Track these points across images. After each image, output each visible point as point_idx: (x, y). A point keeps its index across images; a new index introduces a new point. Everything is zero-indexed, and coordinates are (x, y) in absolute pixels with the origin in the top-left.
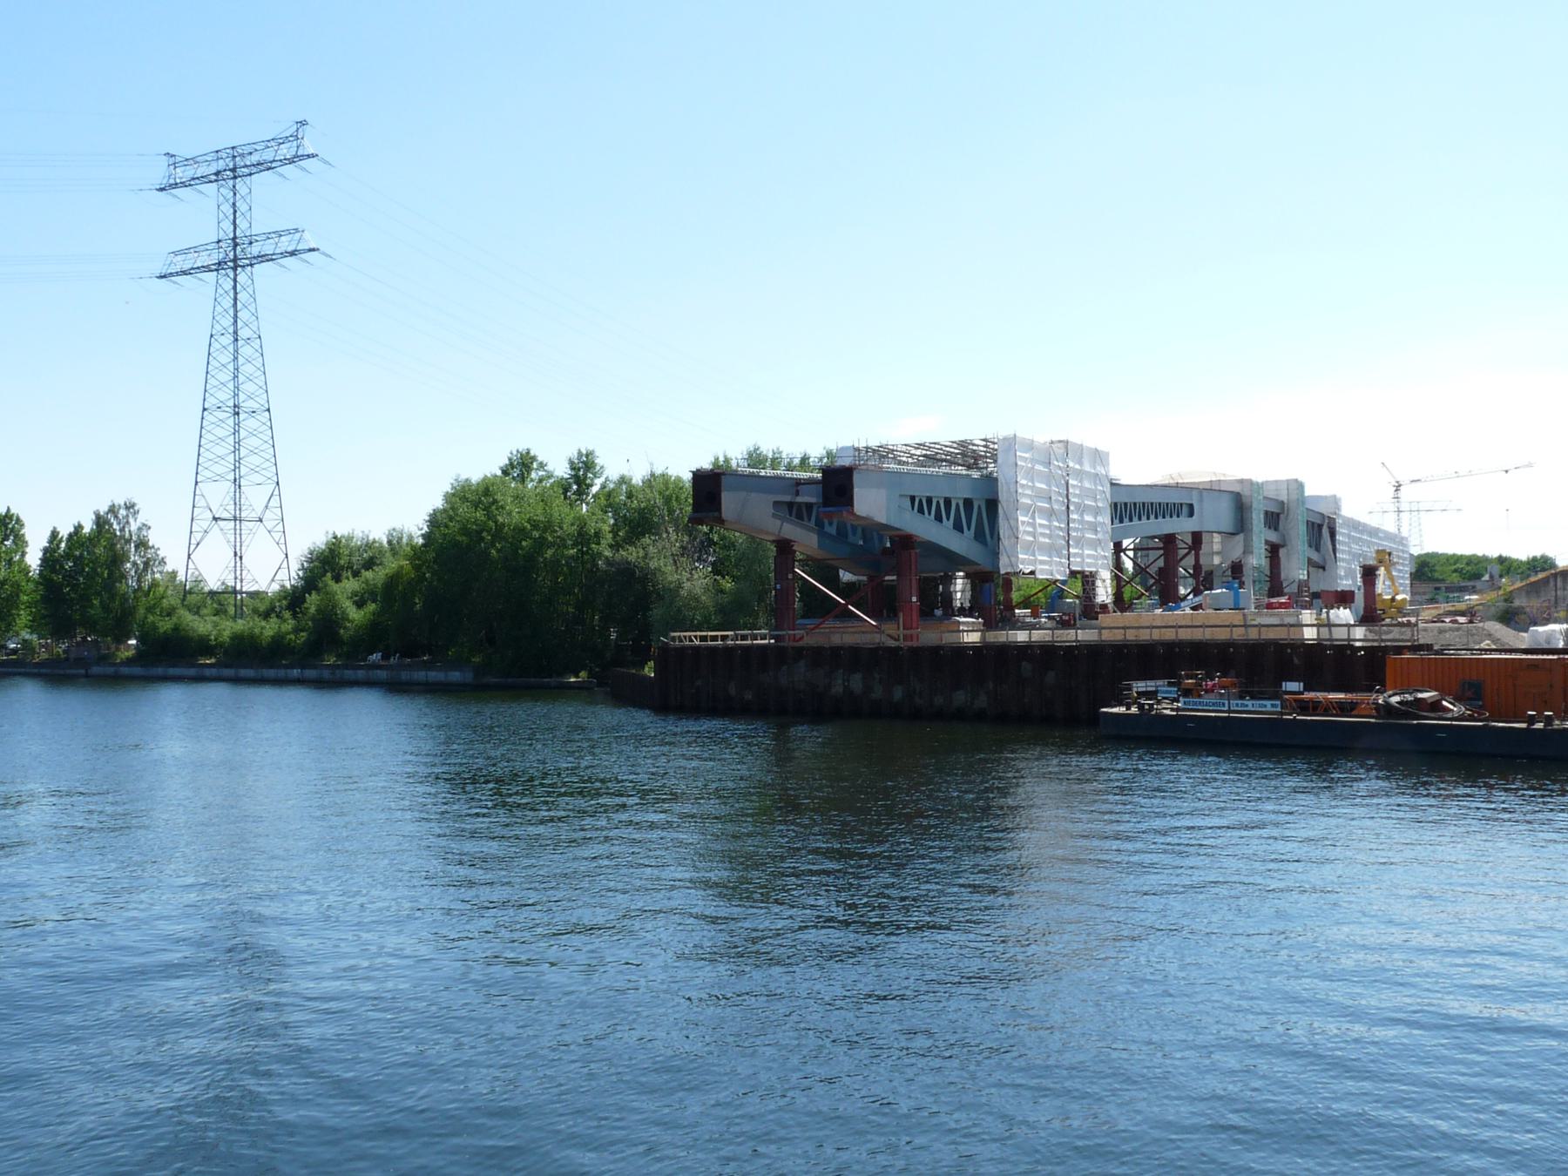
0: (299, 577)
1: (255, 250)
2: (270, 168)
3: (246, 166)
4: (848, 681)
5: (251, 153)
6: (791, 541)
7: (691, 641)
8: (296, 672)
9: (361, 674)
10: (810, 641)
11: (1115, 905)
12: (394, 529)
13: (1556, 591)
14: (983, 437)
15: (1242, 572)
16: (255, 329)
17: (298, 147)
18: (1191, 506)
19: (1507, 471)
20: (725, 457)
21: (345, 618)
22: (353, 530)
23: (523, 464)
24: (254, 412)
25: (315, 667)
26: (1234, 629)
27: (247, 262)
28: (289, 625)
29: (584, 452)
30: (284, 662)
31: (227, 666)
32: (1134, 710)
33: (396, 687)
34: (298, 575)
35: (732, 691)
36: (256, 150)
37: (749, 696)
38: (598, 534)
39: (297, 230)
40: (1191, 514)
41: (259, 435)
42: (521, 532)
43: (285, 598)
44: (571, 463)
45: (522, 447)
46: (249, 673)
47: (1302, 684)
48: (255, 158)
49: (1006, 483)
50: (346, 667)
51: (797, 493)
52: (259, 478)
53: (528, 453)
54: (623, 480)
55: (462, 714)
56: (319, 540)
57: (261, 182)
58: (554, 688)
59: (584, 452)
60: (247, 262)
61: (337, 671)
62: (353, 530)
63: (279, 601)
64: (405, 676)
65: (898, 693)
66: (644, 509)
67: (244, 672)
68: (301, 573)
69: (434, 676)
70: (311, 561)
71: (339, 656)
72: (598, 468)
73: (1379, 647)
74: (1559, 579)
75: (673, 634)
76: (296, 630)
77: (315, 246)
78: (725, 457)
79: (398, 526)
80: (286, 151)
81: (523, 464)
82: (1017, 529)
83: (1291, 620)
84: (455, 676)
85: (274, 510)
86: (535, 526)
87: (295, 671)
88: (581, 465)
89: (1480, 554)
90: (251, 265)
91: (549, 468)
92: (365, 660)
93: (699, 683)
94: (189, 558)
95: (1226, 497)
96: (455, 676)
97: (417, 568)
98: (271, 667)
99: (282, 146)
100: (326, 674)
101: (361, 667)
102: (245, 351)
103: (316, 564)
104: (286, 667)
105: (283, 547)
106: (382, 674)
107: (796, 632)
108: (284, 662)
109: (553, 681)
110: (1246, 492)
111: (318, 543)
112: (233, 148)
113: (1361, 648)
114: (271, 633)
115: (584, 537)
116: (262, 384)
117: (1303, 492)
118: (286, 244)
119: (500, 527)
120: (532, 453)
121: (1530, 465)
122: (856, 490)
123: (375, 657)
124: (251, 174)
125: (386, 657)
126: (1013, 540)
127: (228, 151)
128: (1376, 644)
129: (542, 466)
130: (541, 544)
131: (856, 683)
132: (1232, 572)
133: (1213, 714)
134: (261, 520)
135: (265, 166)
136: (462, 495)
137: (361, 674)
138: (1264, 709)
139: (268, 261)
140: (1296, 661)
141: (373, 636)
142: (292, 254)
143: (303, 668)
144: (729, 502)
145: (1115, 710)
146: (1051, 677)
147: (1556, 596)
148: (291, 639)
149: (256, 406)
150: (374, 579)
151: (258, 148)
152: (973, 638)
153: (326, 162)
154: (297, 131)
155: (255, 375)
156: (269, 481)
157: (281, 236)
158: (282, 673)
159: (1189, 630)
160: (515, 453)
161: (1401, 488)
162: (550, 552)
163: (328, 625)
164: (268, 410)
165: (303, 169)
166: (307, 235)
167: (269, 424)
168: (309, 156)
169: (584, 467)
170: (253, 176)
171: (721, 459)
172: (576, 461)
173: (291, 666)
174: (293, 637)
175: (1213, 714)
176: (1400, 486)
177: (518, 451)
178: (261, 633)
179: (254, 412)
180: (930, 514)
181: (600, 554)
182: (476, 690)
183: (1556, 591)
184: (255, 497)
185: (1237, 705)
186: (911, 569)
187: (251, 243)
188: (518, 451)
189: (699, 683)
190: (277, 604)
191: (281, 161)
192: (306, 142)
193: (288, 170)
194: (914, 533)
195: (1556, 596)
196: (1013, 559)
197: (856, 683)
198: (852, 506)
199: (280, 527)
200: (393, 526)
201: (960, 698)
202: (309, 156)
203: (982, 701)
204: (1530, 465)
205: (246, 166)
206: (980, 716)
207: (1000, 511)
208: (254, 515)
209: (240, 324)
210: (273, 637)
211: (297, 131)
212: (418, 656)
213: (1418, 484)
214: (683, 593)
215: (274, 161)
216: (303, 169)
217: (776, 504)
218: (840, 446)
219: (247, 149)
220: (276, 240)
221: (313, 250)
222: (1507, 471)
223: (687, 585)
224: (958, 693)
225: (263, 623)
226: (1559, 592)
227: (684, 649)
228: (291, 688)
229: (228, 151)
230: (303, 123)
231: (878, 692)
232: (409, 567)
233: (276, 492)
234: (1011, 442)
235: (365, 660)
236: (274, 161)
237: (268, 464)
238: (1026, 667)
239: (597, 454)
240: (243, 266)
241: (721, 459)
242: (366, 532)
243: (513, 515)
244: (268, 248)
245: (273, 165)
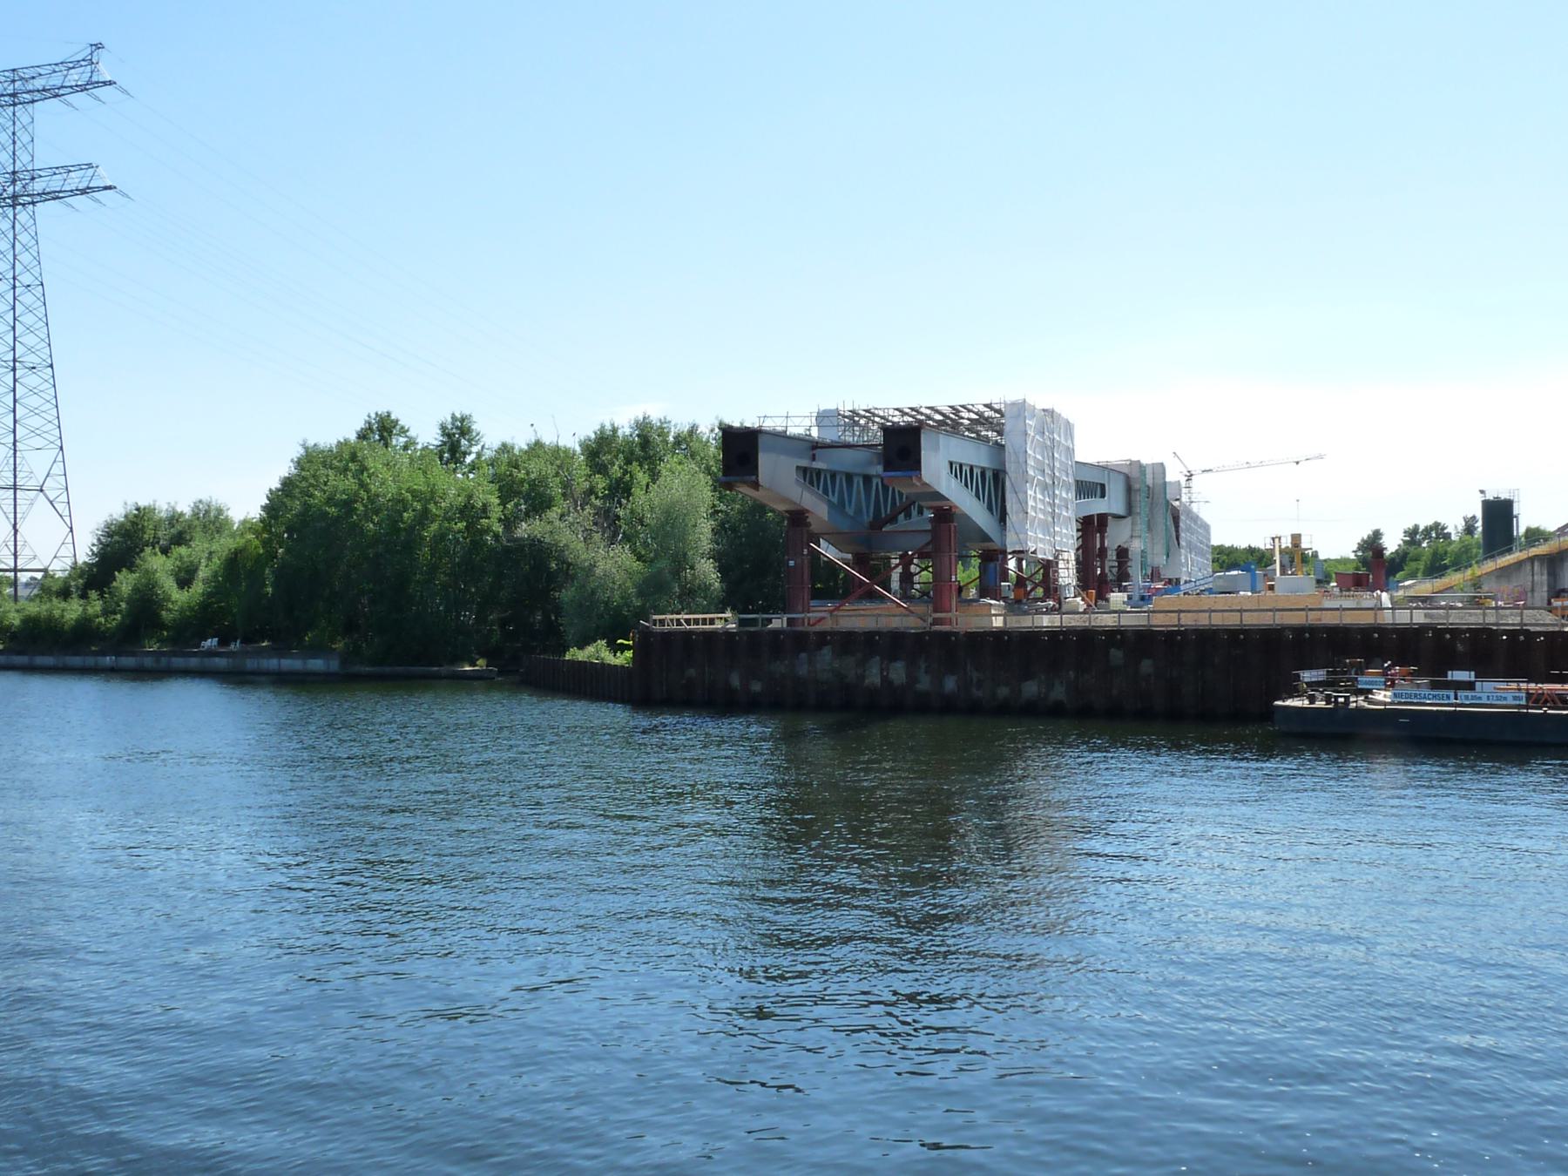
0: (93, 554)
1: (38, 186)
2: (57, 96)
3: (29, 92)
4: (888, 670)
5: (33, 78)
6: (808, 511)
7: (681, 625)
8: (108, 660)
9: (194, 662)
10: (827, 625)
11: (1354, 934)
12: (200, 501)
13: (1533, 575)
14: (988, 402)
15: (1127, 557)
16: (37, 275)
17: (92, 72)
18: (1103, 486)
19: (1297, 463)
20: (613, 425)
21: (168, 599)
22: (155, 501)
23: (383, 428)
24: (34, 368)
25: (133, 654)
26: (1309, 613)
27: (29, 199)
28: (96, 606)
29: (459, 416)
30: (93, 648)
31: (20, 653)
32: (1320, 704)
33: (236, 678)
34: (92, 550)
35: (735, 681)
36: (40, 75)
37: (756, 687)
38: (485, 508)
39: (90, 166)
40: (1103, 496)
41: (43, 414)
42: (400, 503)
43: (81, 576)
44: (443, 428)
45: (382, 410)
46: (49, 660)
47: (1473, 673)
48: (38, 83)
49: (1015, 453)
50: (174, 654)
51: (814, 458)
52: (38, 442)
53: (389, 416)
54: (505, 448)
55: (322, 710)
56: (115, 509)
57: (46, 109)
58: (445, 678)
59: (459, 416)
60: (29, 199)
61: (163, 659)
62: (155, 501)
63: (74, 580)
64: (250, 664)
65: (950, 684)
66: (534, 480)
67: (40, 660)
68: (95, 549)
69: (288, 664)
70: (109, 535)
71: (161, 641)
72: (474, 434)
73: (1179, 630)
74: (1536, 564)
75: (655, 617)
76: (106, 612)
77: (109, 183)
78: (613, 425)
79: (205, 498)
80: (75, 77)
81: (383, 428)
82: (1027, 502)
83: (1370, 603)
84: (317, 664)
85: (58, 478)
86: (415, 494)
87: (108, 658)
88: (454, 431)
89: (1227, 544)
90: (33, 203)
91: (411, 433)
92: (198, 647)
93: (692, 672)
94: (71, 528)
95: (1122, 477)
96: (317, 664)
97: (265, 543)
98: (76, 654)
99: (72, 71)
100: (148, 662)
101: (195, 655)
102: (27, 298)
103: (116, 538)
104: (96, 654)
105: (67, 519)
106: (221, 663)
107: (810, 615)
108: (93, 648)
109: (444, 670)
110: (1135, 474)
111: (115, 516)
112: (14, 70)
113: (1539, 634)
114: (74, 616)
115: (470, 512)
116: (44, 336)
117: (1164, 477)
118: (76, 180)
119: (373, 499)
120: (393, 417)
121: (1321, 457)
122: (923, 452)
123: (210, 643)
124: (33, 101)
125: (224, 642)
126: (1021, 515)
127: (6, 74)
128: (1557, 629)
129: (403, 431)
130: (424, 517)
131: (898, 672)
132: (1118, 557)
133: (1435, 708)
134: (41, 490)
135: (53, 93)
136: (312, 460)
137: (194, 662)
138: (1504, 703)
139: (54, 199)
140: (1460, 647)
141: (202, 621)
142: (84, 192)
143: (118, 654)
144: (765, 461)
145: (1289, 703)
146: (1146, 666)
147: (1533, 581)
148: (100, 623)
149: (38, 360)
150: (190, 556)
151: (42, 72)
152: (998, 622)
153: (125, 92)
154: (91, 54)
155: (36, 326)
156: (52, 446)
157: (70, 171)
158: (90, 661)
159: (1256, 614)
160: (373, 416)
161: (1193, 478)
162: (434, 527)
163: (146, 606)
164: (51, 366)
165: (97, 98)
166: (100, 170)
167: (56, 422)
168: (105, 83)
169: (456, 437)
170: (36, 104)
171: (608, 427)
172: (450, 427)
173: (103, 654)
174: (103, 620)
175: (1435, 708)
176: (1191, 475)
177: (377, 414)
178: (63, 616)
179: (34, 368)
180: (833, 494)
181: (488, 530)
182: (343, 680)
183: (1533, 575)
184: (36, 463)
185: (1467, 697)
186: (950, 545)
187: (33, 179)
188: (377, 414)
189: (692, 672)
190: (73, 584)
191: (71, 87)
192: (101, 66)
193: (78, 99)
194: (958, 505)
195: (1533, 581)
196: (1021, 536)
197: (898, 672)
198: (920, 470)
199: (64, 498)
200: (200, 497)
201: (1031, 689)
202: (105, 83)
203: (1059, 693)
204: (1321, 457)
205: (29, 92)
206: (1055, 712)
207: (1008, 483)
208: (33, 483)
209: (19, 267)
210: (77, 621)
211: (91, 54)
212: (257, 642)
213: (1210, 473)
214: (598, 572)
215: (62, 87)
216: (97, 98)
217: (798, 467)
218: (822, 409)
219: (28, 73)
220: (65, 175)
221: (109, 188)
222: (1297, 463)
223: (601, 564)
224: (1028, 683)
225: (63, 605)
226: (1536, 578)
227: (670, 634)
228: (197, 681)
229: (6, 74)
230: (98, 46)
231: (925, 683)
232: (257, 542)
233: (60, 458)
234: (1021, 408)
235: (198, 647)
236: (62, 87)
237: (50, 426)
238: (1116, 655)
239: (474, 419)
240: (23, 205)
241: (608, 427)
242: (173, 504)
243: (385, 485)
244: (55, 184)
245: (61, 92)
